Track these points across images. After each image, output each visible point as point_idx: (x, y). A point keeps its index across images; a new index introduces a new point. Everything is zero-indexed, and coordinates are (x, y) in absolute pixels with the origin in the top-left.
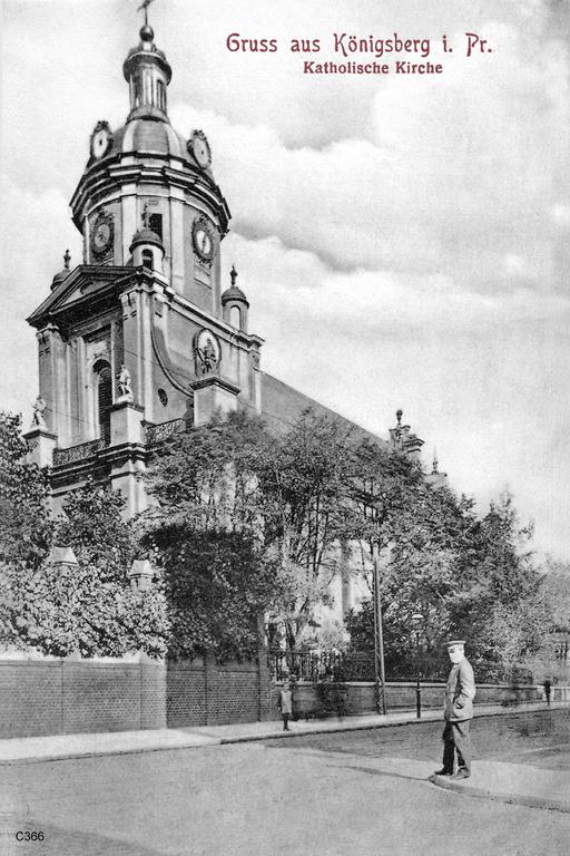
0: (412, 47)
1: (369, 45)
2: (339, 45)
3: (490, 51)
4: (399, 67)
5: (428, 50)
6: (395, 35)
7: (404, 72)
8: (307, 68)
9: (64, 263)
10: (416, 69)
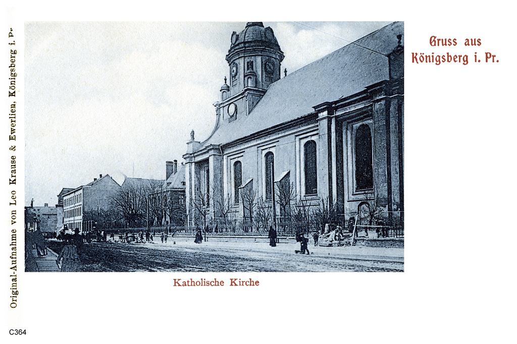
0: (457, 59)
1: (431, 58)
2: (415, 59)
3: (498, 61)
4: (233, 282)
5: (467, 61)
6: (215, 279)
7: (236, 285)
8: (176, 283)
9: (224, 81)
10: (244, 283)
